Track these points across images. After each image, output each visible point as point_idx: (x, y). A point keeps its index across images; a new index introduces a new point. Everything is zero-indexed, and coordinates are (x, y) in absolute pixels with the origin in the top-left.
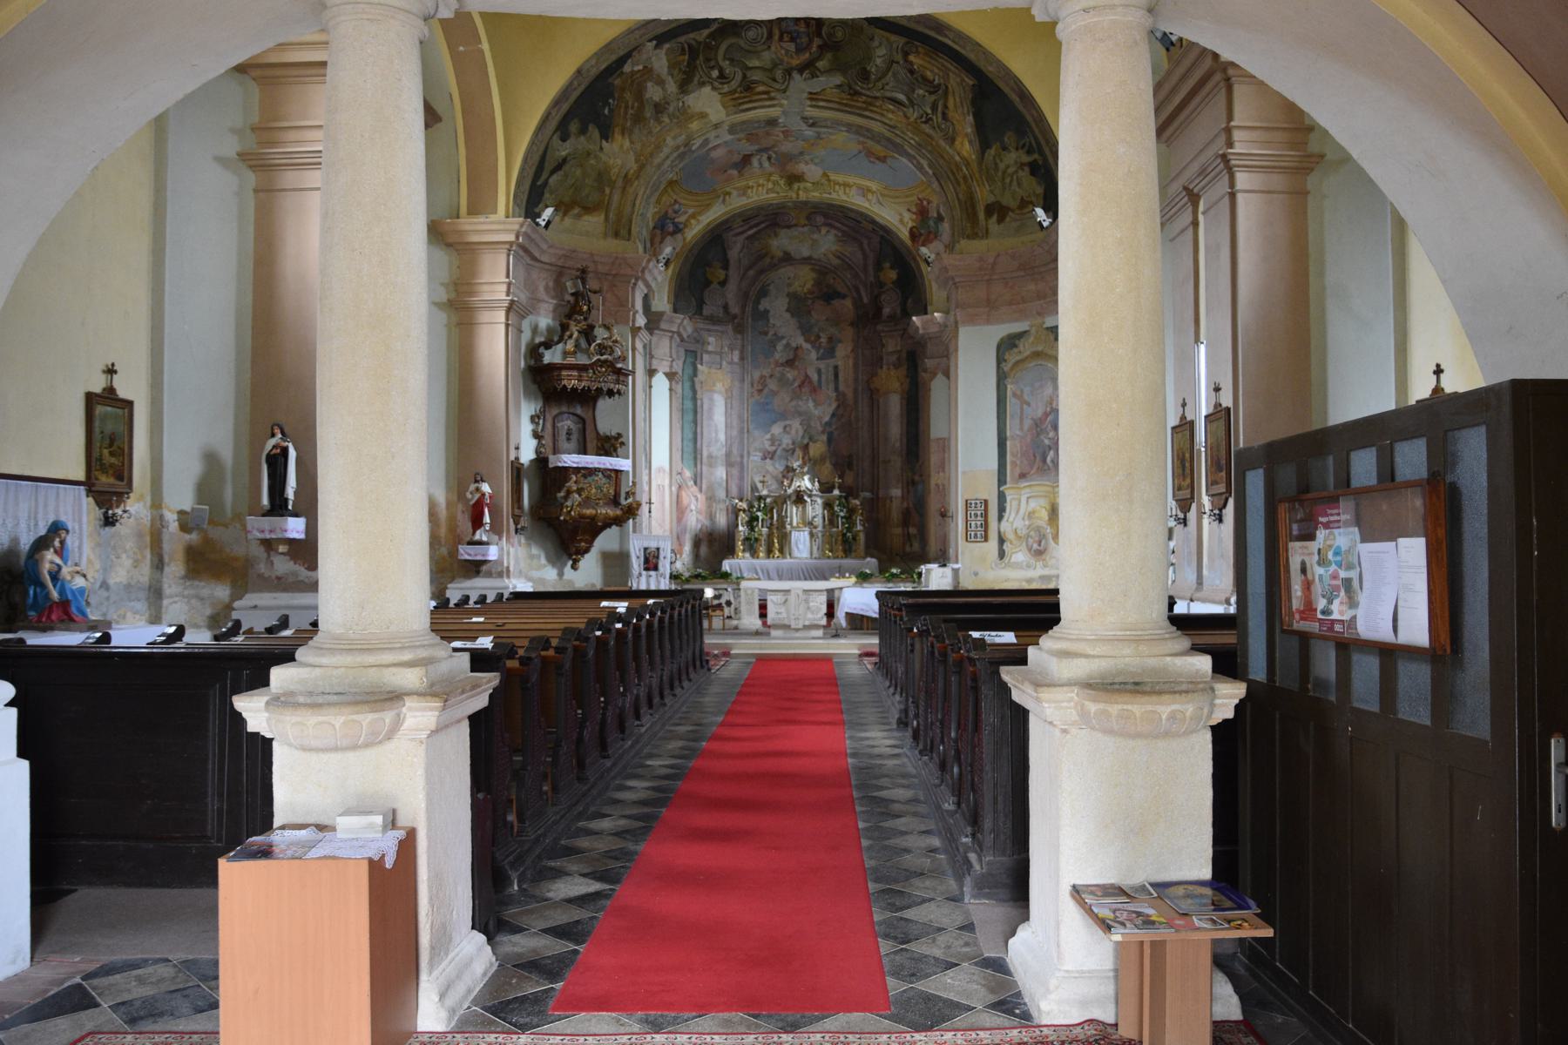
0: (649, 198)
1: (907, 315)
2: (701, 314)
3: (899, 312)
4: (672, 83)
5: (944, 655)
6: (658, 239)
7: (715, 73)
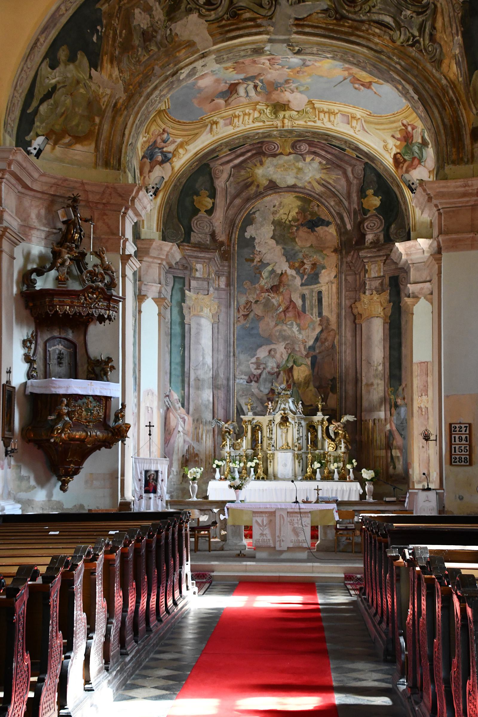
1: (389, 240)
3: (382, 237)
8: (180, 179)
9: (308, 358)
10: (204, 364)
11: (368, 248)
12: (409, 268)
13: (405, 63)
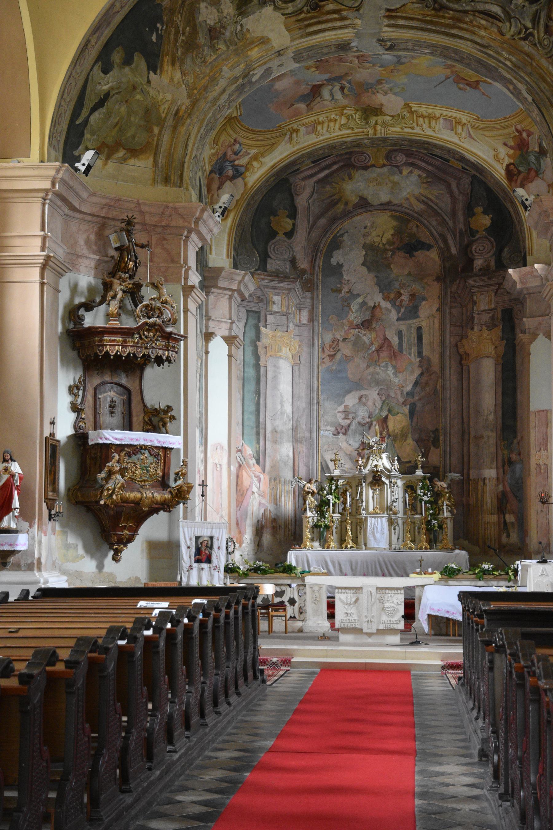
0: (203, 138)
1: (502, 267)
2: (265, 270)
3: (493, 263)
5: (521, 676)
6: (215, 185)
8: (254, 196)
9: (405, 406)
10: (282, 413)
11: (476, 275)
12: (525, 298)
13: (516, 59)
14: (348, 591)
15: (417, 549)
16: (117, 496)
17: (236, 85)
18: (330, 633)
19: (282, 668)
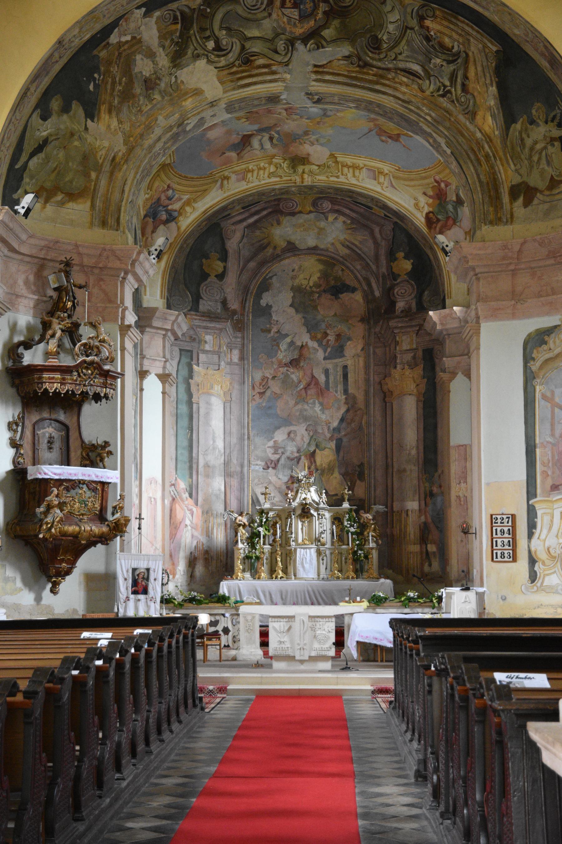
0: (140, 183)
1: (422, 309)
2: (197, 310)
3: (414, 305)
4: (163, 54)
5: (465, 699)
7: (211, 45)
9: (332, 441)
10: (214, 449)
11: (398, 317)
12: (444, 339)
14: (281, 620)
15: (344, 579)
16: (55, 529)
17: (171, 133)
18: (263, 660)
19: (219, 695)
